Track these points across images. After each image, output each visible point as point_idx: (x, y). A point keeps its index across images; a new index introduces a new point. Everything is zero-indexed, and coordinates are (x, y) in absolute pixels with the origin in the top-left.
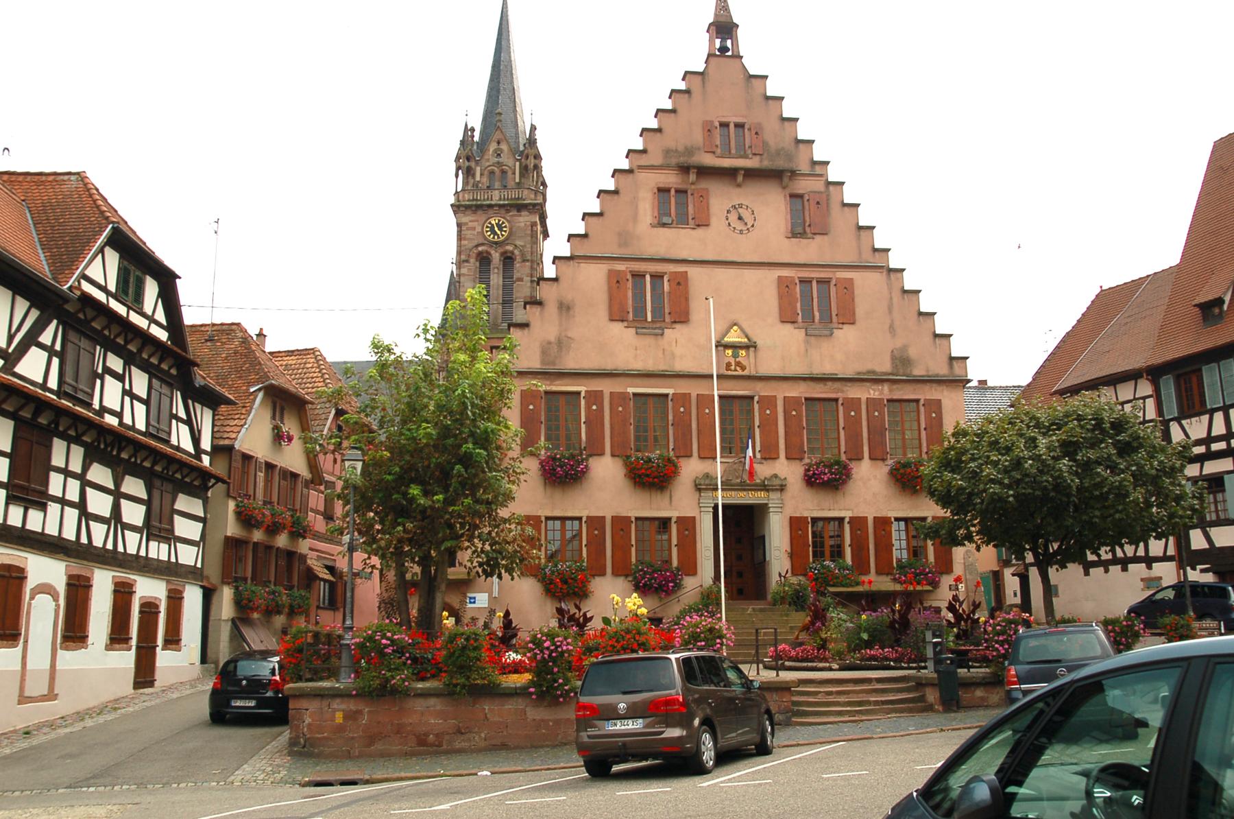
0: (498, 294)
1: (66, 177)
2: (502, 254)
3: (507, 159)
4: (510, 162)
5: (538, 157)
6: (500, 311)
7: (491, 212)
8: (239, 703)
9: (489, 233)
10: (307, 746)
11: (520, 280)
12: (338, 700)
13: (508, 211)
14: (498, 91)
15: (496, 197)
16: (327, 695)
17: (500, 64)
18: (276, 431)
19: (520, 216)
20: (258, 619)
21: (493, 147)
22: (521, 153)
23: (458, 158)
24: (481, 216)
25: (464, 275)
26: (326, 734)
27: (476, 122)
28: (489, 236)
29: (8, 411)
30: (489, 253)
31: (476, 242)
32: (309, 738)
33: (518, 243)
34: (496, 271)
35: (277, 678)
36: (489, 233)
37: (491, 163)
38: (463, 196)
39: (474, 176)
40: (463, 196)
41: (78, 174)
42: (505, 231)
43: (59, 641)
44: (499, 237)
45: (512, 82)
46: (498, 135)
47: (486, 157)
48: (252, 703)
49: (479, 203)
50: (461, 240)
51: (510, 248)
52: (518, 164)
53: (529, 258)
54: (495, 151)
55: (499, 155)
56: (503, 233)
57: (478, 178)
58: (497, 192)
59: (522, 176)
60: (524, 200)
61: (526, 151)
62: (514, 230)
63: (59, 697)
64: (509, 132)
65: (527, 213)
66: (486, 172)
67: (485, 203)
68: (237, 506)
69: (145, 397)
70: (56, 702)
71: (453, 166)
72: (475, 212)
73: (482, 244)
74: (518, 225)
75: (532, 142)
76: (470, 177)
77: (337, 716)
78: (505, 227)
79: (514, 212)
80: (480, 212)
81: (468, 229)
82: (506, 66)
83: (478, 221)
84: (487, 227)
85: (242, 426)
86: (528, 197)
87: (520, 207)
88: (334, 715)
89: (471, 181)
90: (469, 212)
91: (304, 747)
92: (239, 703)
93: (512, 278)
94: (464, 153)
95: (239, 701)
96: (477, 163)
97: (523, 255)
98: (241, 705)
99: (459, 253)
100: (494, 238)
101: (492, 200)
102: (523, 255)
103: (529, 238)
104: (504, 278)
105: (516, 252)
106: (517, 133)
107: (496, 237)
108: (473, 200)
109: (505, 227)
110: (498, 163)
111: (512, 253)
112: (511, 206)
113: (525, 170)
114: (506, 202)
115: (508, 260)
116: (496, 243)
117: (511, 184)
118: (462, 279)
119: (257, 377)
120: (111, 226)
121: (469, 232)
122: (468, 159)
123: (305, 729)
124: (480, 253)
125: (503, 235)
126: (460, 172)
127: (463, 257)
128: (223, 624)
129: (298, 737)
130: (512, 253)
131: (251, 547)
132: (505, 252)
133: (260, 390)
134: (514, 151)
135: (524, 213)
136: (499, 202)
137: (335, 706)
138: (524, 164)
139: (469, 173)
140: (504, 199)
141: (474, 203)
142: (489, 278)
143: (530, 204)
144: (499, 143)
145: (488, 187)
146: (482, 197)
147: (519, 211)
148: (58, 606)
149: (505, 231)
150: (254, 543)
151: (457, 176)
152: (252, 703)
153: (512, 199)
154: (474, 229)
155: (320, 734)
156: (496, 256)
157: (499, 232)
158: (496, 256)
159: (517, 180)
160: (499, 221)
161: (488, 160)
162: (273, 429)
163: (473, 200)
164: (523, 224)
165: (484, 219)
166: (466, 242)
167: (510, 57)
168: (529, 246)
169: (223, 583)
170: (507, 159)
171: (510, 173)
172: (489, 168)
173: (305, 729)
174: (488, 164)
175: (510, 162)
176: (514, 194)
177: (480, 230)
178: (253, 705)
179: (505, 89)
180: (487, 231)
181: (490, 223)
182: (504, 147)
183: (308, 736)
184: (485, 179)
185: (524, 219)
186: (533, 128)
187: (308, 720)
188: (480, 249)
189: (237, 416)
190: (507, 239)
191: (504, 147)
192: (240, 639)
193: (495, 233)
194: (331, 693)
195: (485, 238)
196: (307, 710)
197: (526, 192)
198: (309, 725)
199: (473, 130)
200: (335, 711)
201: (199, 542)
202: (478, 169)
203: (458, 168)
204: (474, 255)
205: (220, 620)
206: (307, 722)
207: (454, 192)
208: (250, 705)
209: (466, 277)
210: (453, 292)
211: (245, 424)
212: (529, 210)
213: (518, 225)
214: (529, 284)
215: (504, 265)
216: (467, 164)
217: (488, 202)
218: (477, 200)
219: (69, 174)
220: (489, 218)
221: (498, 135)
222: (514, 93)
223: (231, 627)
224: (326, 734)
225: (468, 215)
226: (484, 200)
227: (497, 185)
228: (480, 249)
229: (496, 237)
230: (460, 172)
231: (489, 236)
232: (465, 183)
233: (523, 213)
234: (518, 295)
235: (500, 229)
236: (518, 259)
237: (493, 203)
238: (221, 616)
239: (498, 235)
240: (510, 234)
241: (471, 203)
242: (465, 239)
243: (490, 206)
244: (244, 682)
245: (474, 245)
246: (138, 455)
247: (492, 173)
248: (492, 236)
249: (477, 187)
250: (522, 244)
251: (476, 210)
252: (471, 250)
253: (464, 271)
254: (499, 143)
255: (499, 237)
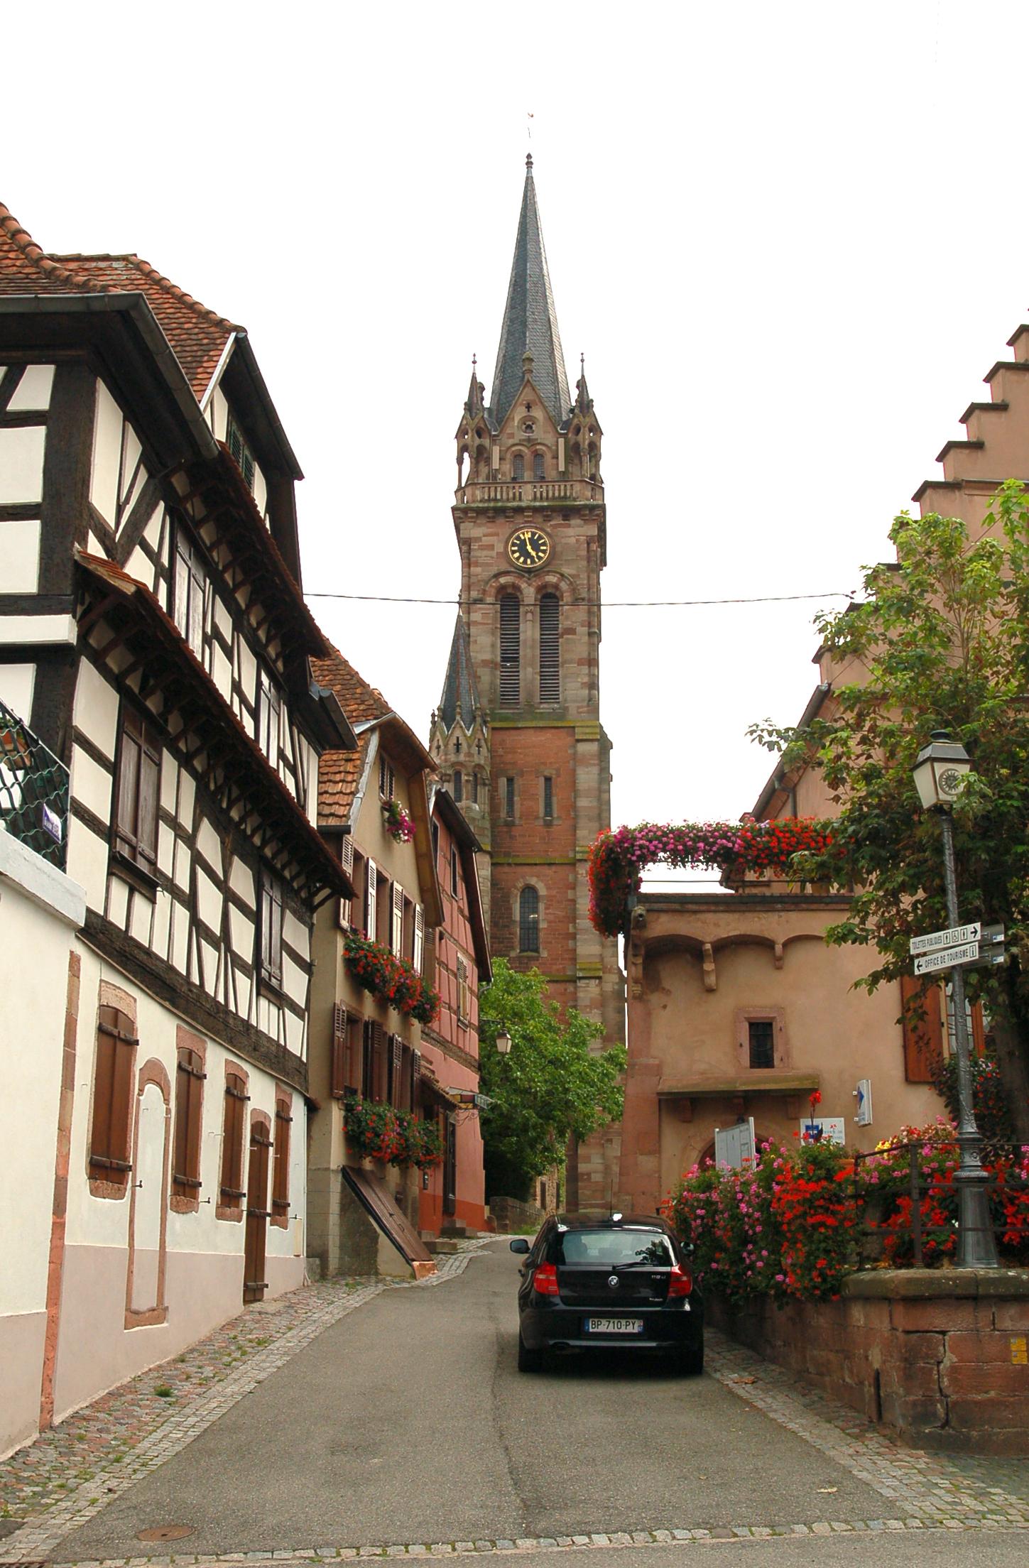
0: (533, 656)
1: (102, 265)
2: (540, 589)
3: (542, 433)
4: (549, 439)
5: (596, 429)
6: (538, 682)
7: (519, 520)
8: (605, 1327)
9: (517, 555)
10: (954, 1423)
11: (571, 631)
12: (1013, 1310)
13: (547, 519)
14: (524, 324)
15: (527, 495)
16: (987, 1297)
17: (525, 281)
18: (387, 814)
19: (569, 526)
20: (372, 1172)
21: (519, 414)
22: (566, 425)
23: (461, 433)
24: (503, 528)
25: (476, 623)
26: (992, 1394)
27: (488, 378)
28: (518, 559)
29: (111, 670)
30: (517, 588)
31: (494, 570)
32: (955, 1404)
33: (566, 570)
34: (529, 616)
35: (676, 1269)
36: (517, 555)
37: (516, 441)
38: (473, 495)
39: (488, 461)
40: (473, 495)
41: (124, 258)
42: (544, 552)
43: (169, 1193)
44: (533, 562)
45: (546, 310)
46: (527, 395)
47: (509, 431)
48: (635, 1327)
49: (500, 504)
50: (469, 566)
51: (552, 579)
52: (561, 441)
53: (584, 595)
54: (523, 421)
55: (529, 427)
56: (541, 554)
57: (496, 465)
58: (529, 486)
59: (568, 460)
60: (575, 500)
61: (576, 421)
62: (559, 549)
63: (170, 1315)
64: (545, 391)
65: (578, 521)
66: (509, 456)
67: (509, 504)
68: (348, 949)
69: (111, 756)
70: (165, 1325)
71: (453, 447)
72: (492, 520)
73: (506, 573)
74: (564, 541)
75: (585, 405)
76: (482, 464)
77: (1013, 1348)
78: (544, 544)
79: (558, 521)
80: (501, 520)
81: (482, 548)
82: (535, 284)
83: (497, 534)
84: (514, 545)
85: (353, 794)
86: (582, 496)
87: (568, 512)
88: (1007, 1347)
89: (484, 470)
90: (482, 520)
91: (946, 1423)
92: (605, 1327)
93: (556, 629)
94: (473, 424)
95: (604, 1322)
96: (494, 440)
97: (574, 590)
98: (611, 1329)
99: (467, 587)
100: (525, 562)
101: (520, 500)
102: (574, 590)
103: (585, 563)
104: (542, 629)
105: (564, 586)
106: (557, 393)
107: (529, 561)
108: (489, 500)
109: (544, 544)
110: (529, 440)
111: (556, 587)
112: (552, 509)
113: (574, 452)
114: (546, 504)
115: (549, 600)
116: (529, 571)
117: (551, 474)
118: (473, 630)
119: (362, 707)
120: (233, 335)
121: (485, 553)
122: (479, 433)
123: (946, 1382)
124: (502, 588)
125: (540, 558)
126: (466, 455)
127: (474, 594)
128: (332, 1175)
129: (929, 1401)
130: (556, 587)
131: (361, 1027)
132: (544, 586)
133: (372, 729)
134: (553, 421)
135: (575, 522)
136: (533, 504)
137: (1008, 1324)
138: (572, 442)
139: (480, 456)
140: (547, 498)
141: (492, 504)
142: (518, 629)
143: (585, 506)
144: (529, 407)
145: (514, 479)
146: (502, 495)
147: (566, 518)
148: (168, 1111)
149: (544, 552)
150: (366, 1024)
151: (460, 461)
152: (635, 1327)
153: (554, 498)
154: (491, 547)
155: (979, 1392)
156: (529, 593)
157: (533, 554)
158: (529, 593)
159: (562, 468)
160: (533, 534)
161: (512, 436)
162: (383, 809)
163: (489, 500)
164: (573, 540)
165: (510, 531)
166: (479, 570)
167: (542, 269)
168: (584, 576)
169: (332, 1096)
170: (542, 433)
171: (548, 456)
172: (514, 449)
173: (946, 1382)
174: (511, 442)
175: (549, 439)
176: (558, 490)
177: (502, 550)
178: (636, 1331)
179: (535, 321)
180: (514, 552)
181: (518, 538)
182: (538, 413)
183: (954, 1397)
184: (507, 467)
185: (576, 532)
186: (582, 385)
187: (949, 1359)
188: (503, 580)
189: (338, 777)
190: (548, 563)
191: (538, 413)
192: (362, 1209)
193: (527, 555)
194: (1002, 1290)
195: (511, 563)
196: (944, 1333)
197: (577, 487)
198: (954, 1369)
199: (483, 389)
200: (1006, 1335)
201: (304, 1011)
202: (496, 451)
203: (462, 449)
204: (493, 591)
205: (328, 1169)
206: (947, 1363)
207: (455, 487)
208: (630, 1329)
209: (481, 627)
210: (462, 649)
211: (357, 791)
212: (581, 516)
213: (564, 541)
214: (586, 638)
215: (542, 608)
216: (477, 441)
217: (515, 504)
218: (495, 500)
219: (106, 258)
220: (517, 530)
221: (527, 395)
222: (550, 327)
223: (342, 1185)
224: (992, 1394)
225: (479, 526)
226: (508, 500)
227: (527, 475)
228: (503, 580)
229: (529, 561)
230: (466, 455)
231: (518, 559)
232: (475, 471)
233: (573, 522)
234: (568, 656)
235: (536, 547)
236: (567, 597)
237: (523, 504)
238: (329, 1163)
239: (532, 558)
240: (553, 555)
241: (486, 505)
242: (477, 564)
243: (519, 510)
244: (614, 1280)
245: (492, 573)
246: (249, 821)
247: (519, 456)
248: (522, 559)
249: (495, 477)
250: (573, 572)
251: (494, 517)
252: (487, 583)
253: (476, 616)
254: (529, 407)
255: (533, 562)
